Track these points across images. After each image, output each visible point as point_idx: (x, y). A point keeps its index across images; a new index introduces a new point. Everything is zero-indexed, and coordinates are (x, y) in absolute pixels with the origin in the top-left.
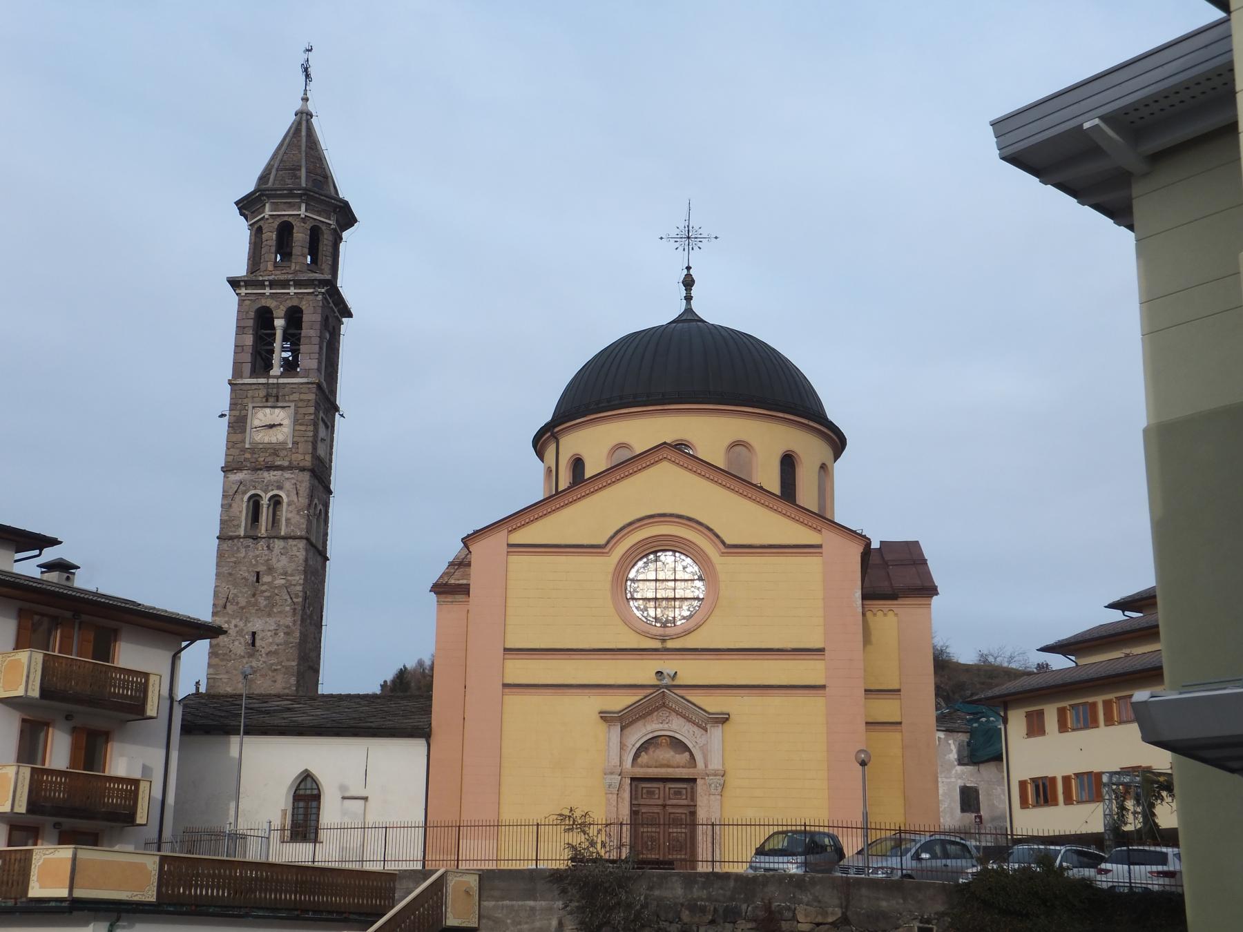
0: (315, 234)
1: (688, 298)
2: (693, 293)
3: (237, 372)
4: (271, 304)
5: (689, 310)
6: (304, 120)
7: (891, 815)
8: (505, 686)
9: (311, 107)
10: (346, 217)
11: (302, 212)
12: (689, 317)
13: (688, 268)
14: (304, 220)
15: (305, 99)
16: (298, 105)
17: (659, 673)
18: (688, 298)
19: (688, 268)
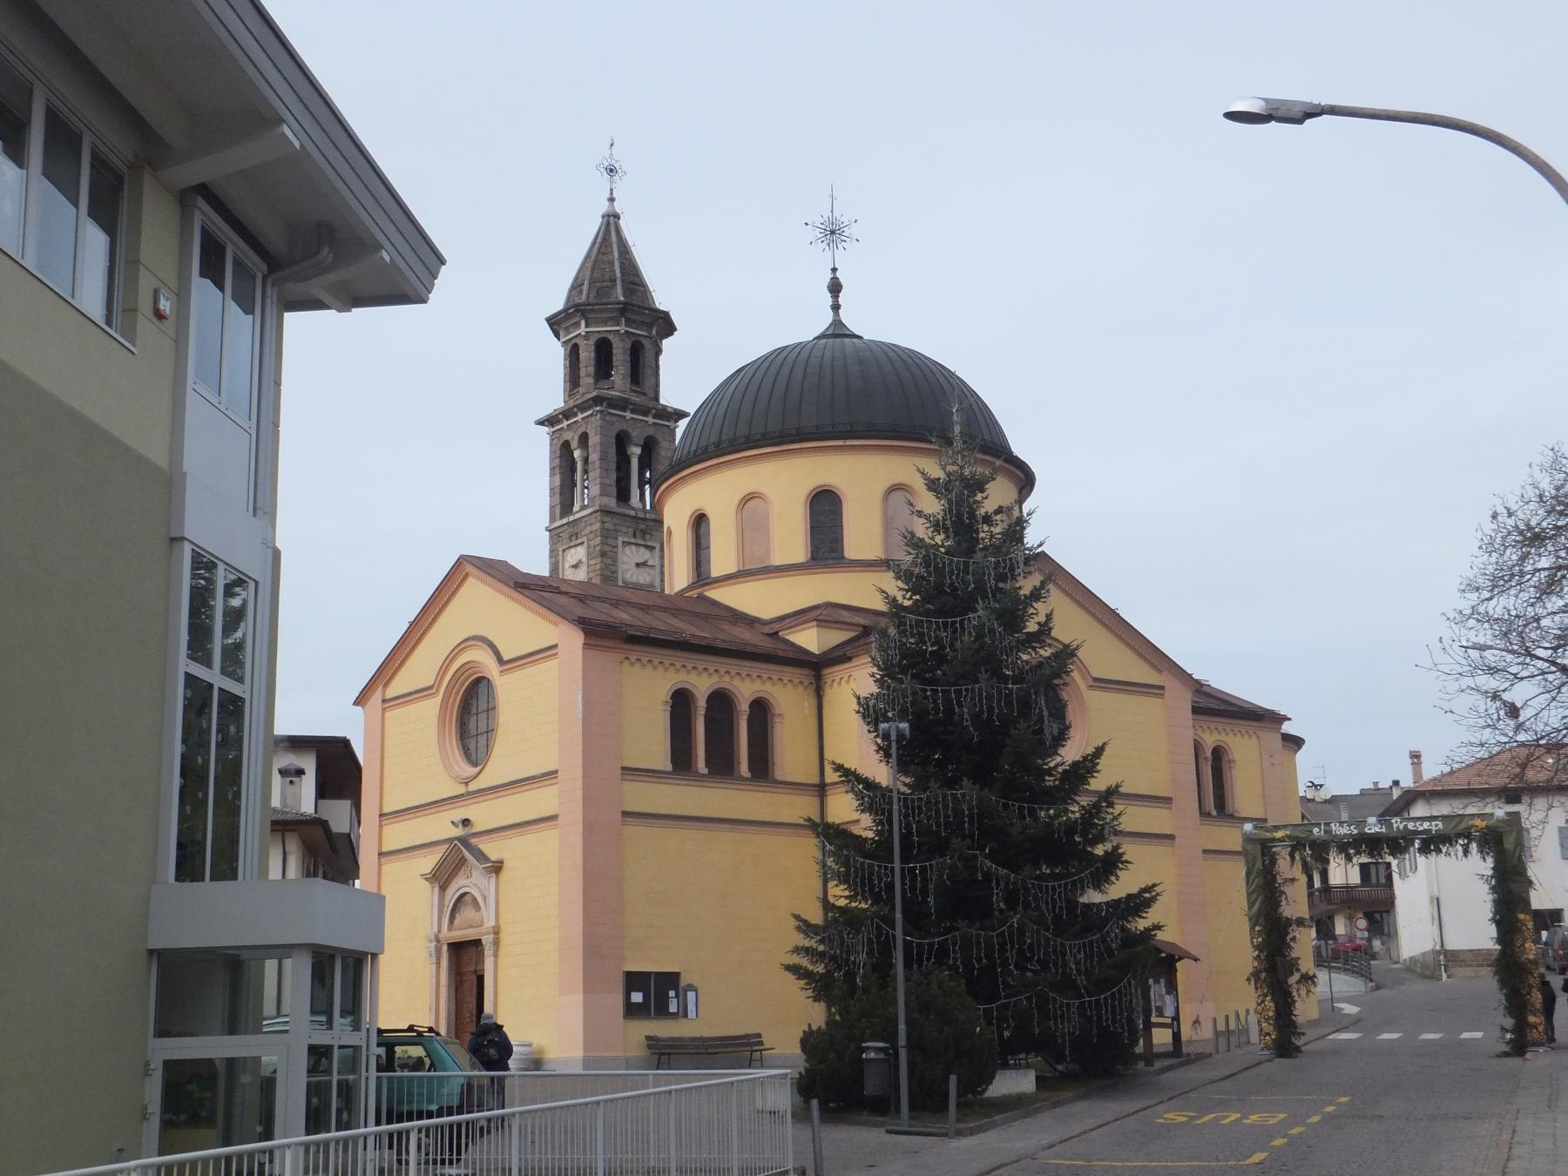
0: (636, 352)
1: (836, 307)
2: (841, 300)
3: (552, 519)
4: (567, 436)
5: (837, 323)
6: (611, 221)
7: (1132, 818)
8: (625, 814)
9: (618, 208)
10: (665, 325)
11: (583, 329)
12: (838, 331)
13: (834, 270)
14: (587, 335)
15: (612, 200)
16: (605, 207)
17: (466, 822)
18: (836, 307)
19: (834, 270)
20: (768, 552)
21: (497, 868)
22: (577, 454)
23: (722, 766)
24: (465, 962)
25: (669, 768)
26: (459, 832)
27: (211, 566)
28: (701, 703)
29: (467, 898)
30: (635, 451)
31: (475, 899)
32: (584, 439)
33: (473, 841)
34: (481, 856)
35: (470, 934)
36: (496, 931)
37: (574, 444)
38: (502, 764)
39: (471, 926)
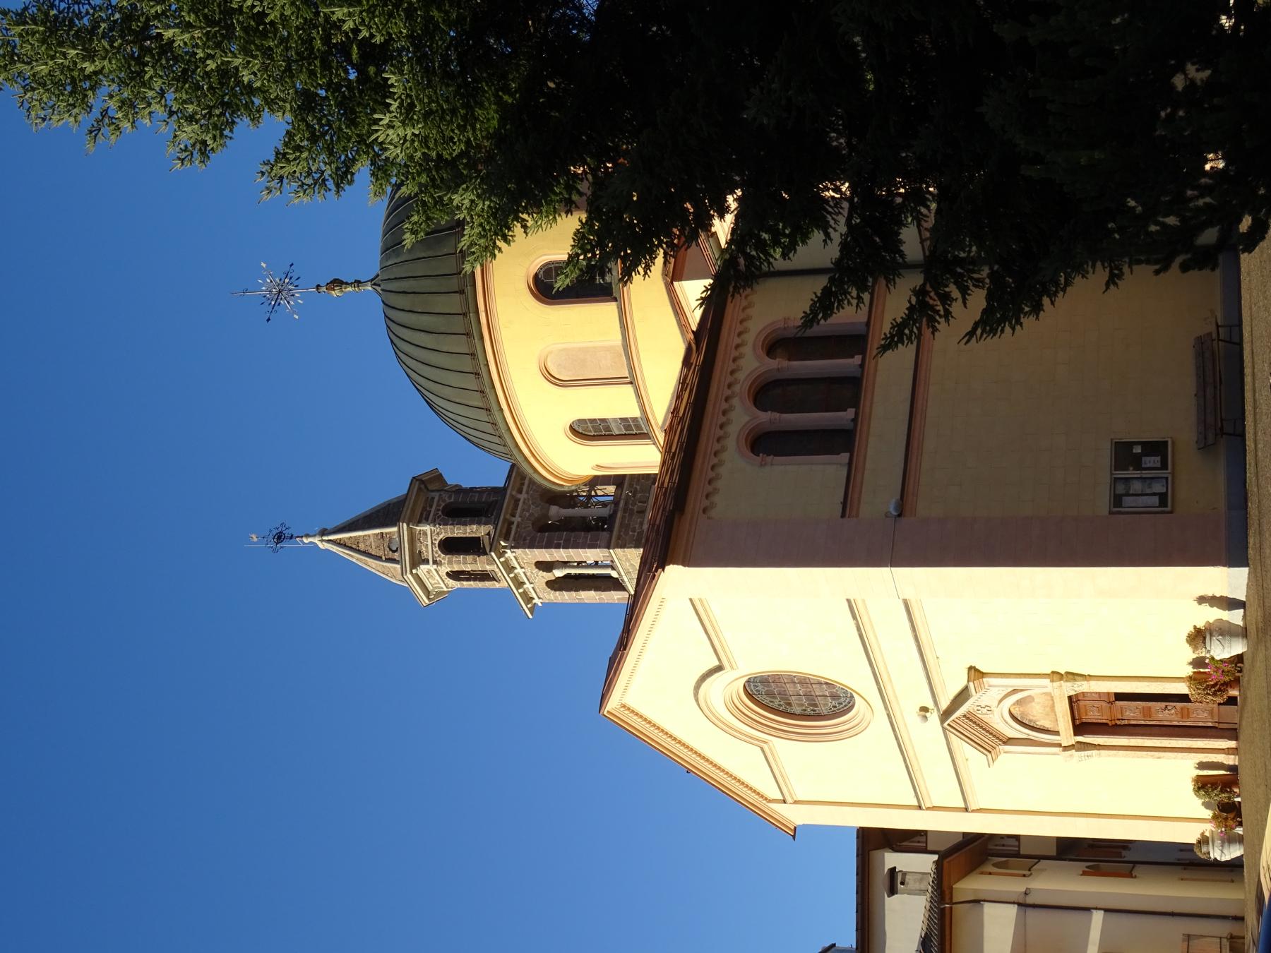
20: (608, 349)
21: (975, 673)
22: (559, 573)
23: (849, 390)
24: (1107, 718)
25: (845, 457)
26: (934, 718)
27: (1236, 682)
28: (765, 417)
29: (1016, 712)
30: (554, 510)
31: (1019, 702)
32: (545, 566)
33: (944, 704)
34: (963, 696)
35: (1063, 709)
36: (1056, 676)
37: (549, 576)
38: (844, 668)
39: (1053, 707)
